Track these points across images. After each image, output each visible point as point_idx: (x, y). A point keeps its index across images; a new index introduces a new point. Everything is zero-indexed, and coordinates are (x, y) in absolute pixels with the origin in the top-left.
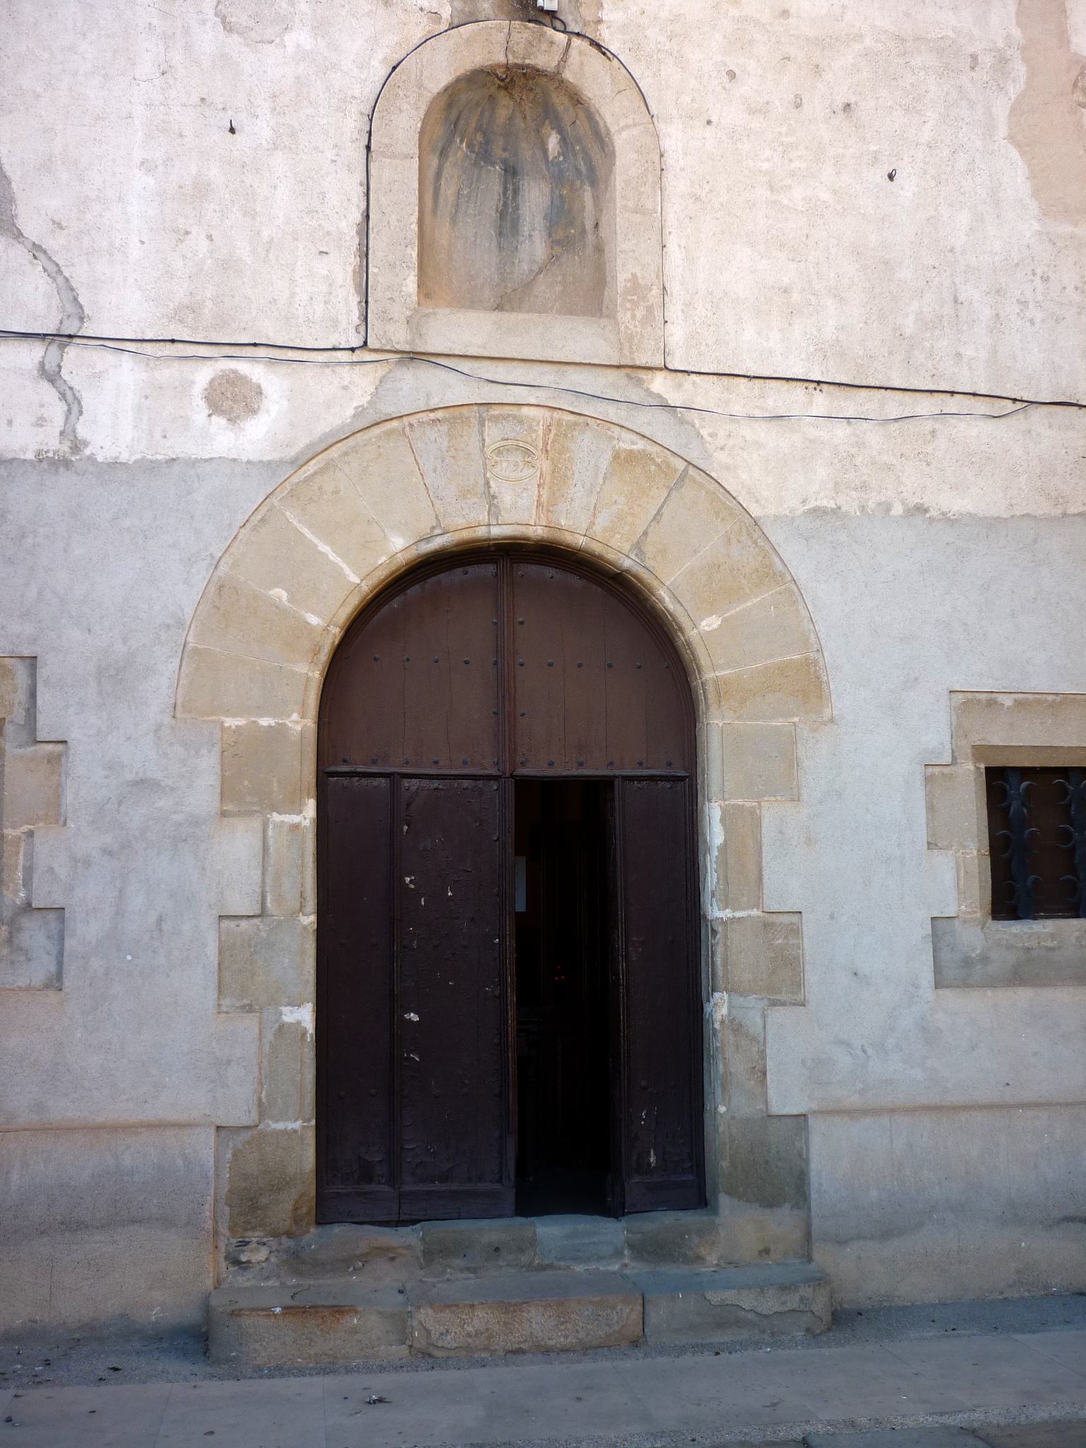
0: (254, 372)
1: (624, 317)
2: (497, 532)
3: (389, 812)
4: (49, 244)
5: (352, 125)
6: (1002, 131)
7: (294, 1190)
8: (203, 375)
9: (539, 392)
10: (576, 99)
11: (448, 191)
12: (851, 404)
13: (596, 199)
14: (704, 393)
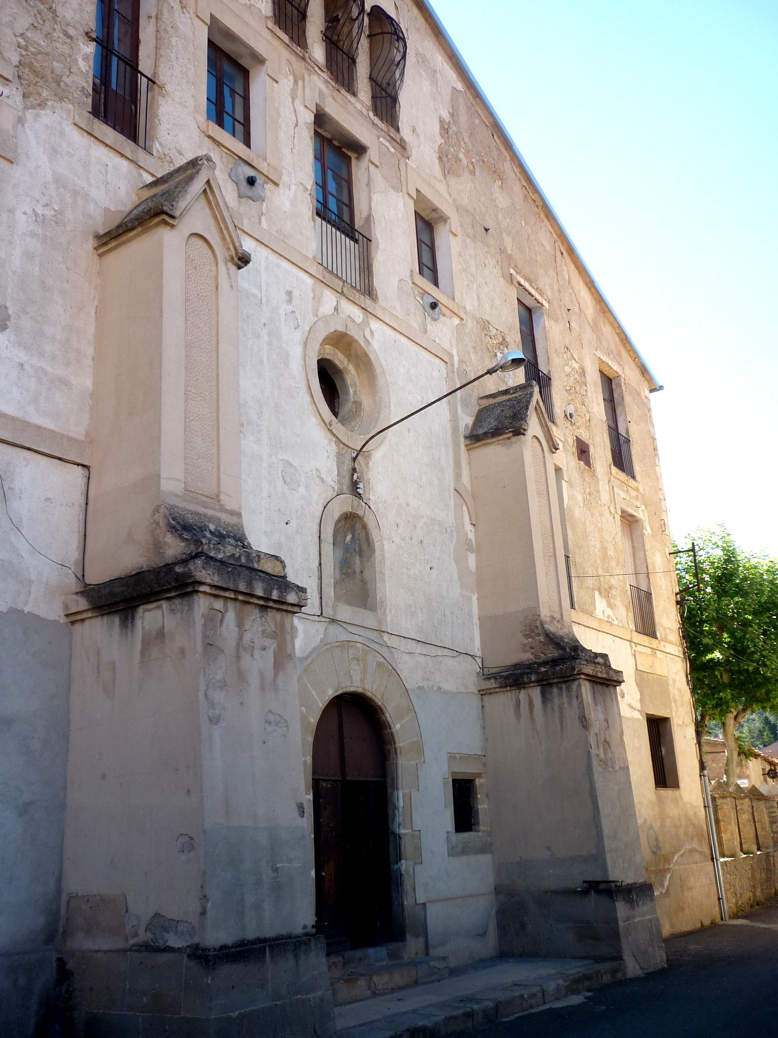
1: (379, 612)
7: (729, 697)
9: (361, 638)
10: (365, 527)
12: (426, 649)
13: (362, 562)
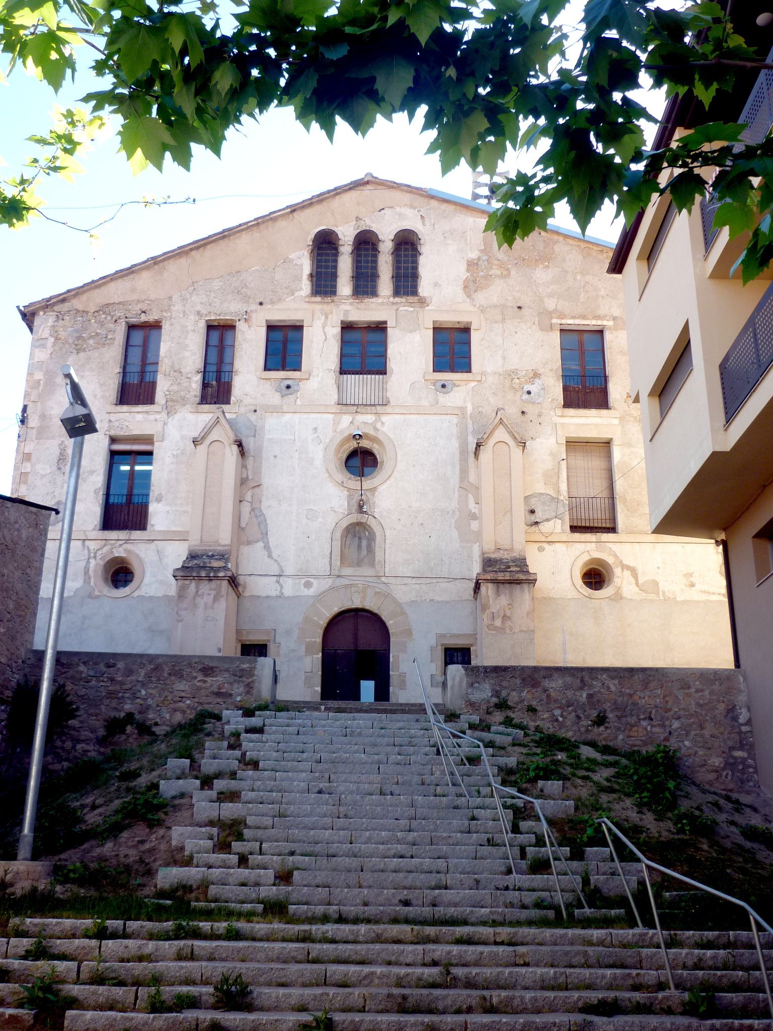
0: (312, 580)
2: (353, 607)
3: (152, 417)
4: (278, 559)
5: (329, 535)
6: (453, 526)
8: (303, 581)
11: (348, 543)
12: (419, 581)
14: (392, 580)
